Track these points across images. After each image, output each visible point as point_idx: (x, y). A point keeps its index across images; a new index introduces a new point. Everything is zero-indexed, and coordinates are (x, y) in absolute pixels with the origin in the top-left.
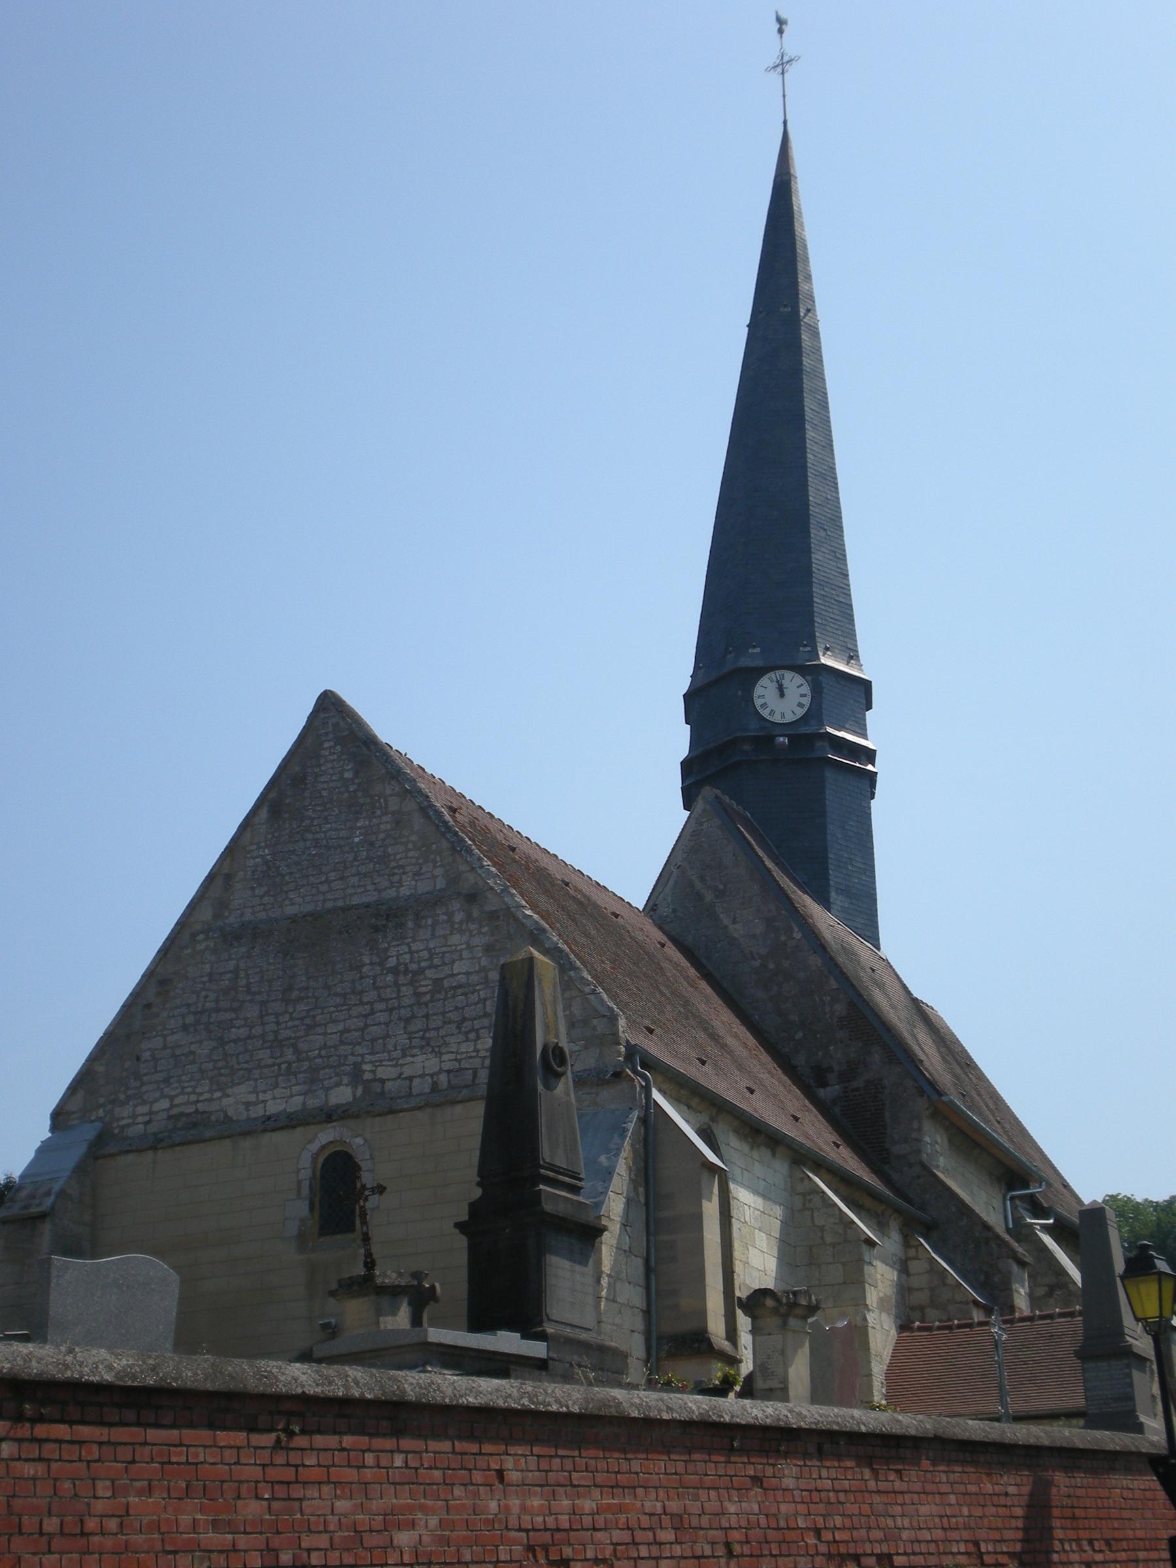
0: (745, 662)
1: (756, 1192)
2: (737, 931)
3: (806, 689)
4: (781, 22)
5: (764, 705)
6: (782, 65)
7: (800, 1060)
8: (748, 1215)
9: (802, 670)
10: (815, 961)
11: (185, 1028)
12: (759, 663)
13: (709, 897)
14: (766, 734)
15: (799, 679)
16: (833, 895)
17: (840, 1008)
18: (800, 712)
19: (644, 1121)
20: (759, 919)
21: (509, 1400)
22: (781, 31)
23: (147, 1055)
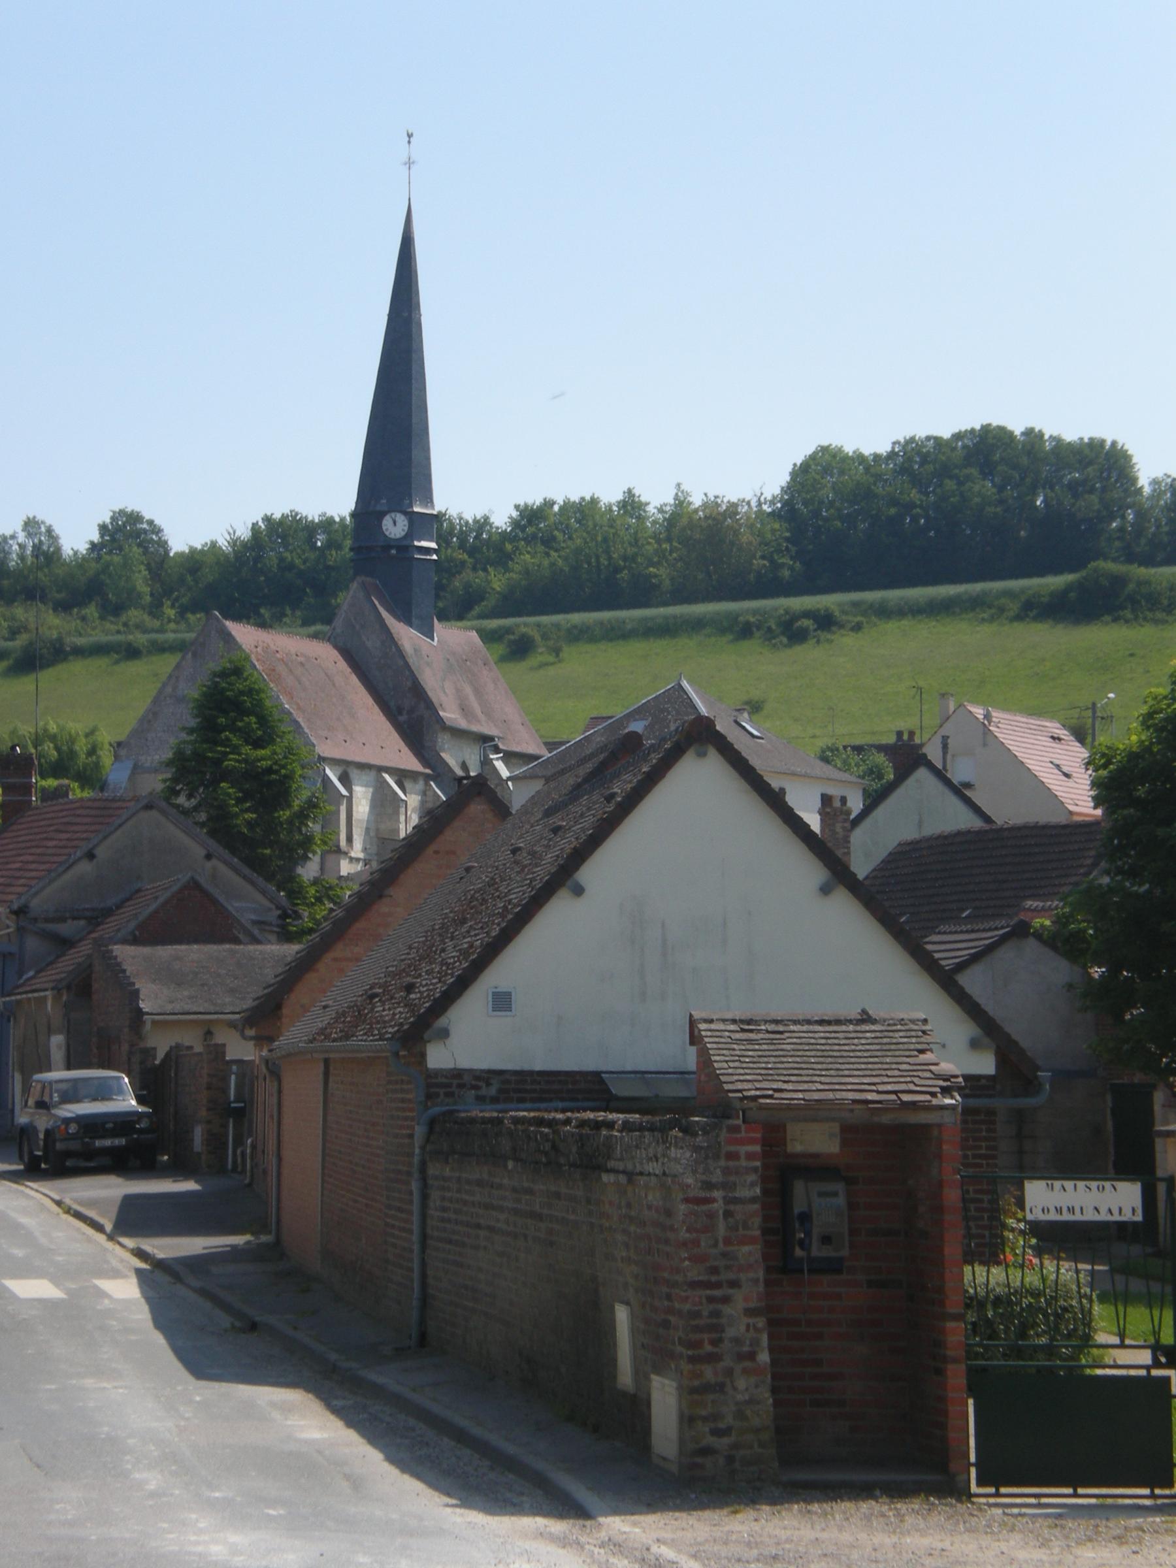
0: (378, 508)
1: (362, 786)
2: (369, 644)
3: (406, 523)
4: (410, 136)
5: (387, 530)
6: (409, 163)
7: (392, 704)
8: (359, 795)
9: (405, 513)
10: (401, 663)
11: (164, 731)
12: (386, 509)
13: (358, 627)
14: (389, 544)
15: (403, 517)
16: (414, 620)
17: (409, 684)
18: (403, 534)
19: (323, 781)
20: (172, 1495)
21: (418, 995)
22: (409, 142)
23: (149, 739)
